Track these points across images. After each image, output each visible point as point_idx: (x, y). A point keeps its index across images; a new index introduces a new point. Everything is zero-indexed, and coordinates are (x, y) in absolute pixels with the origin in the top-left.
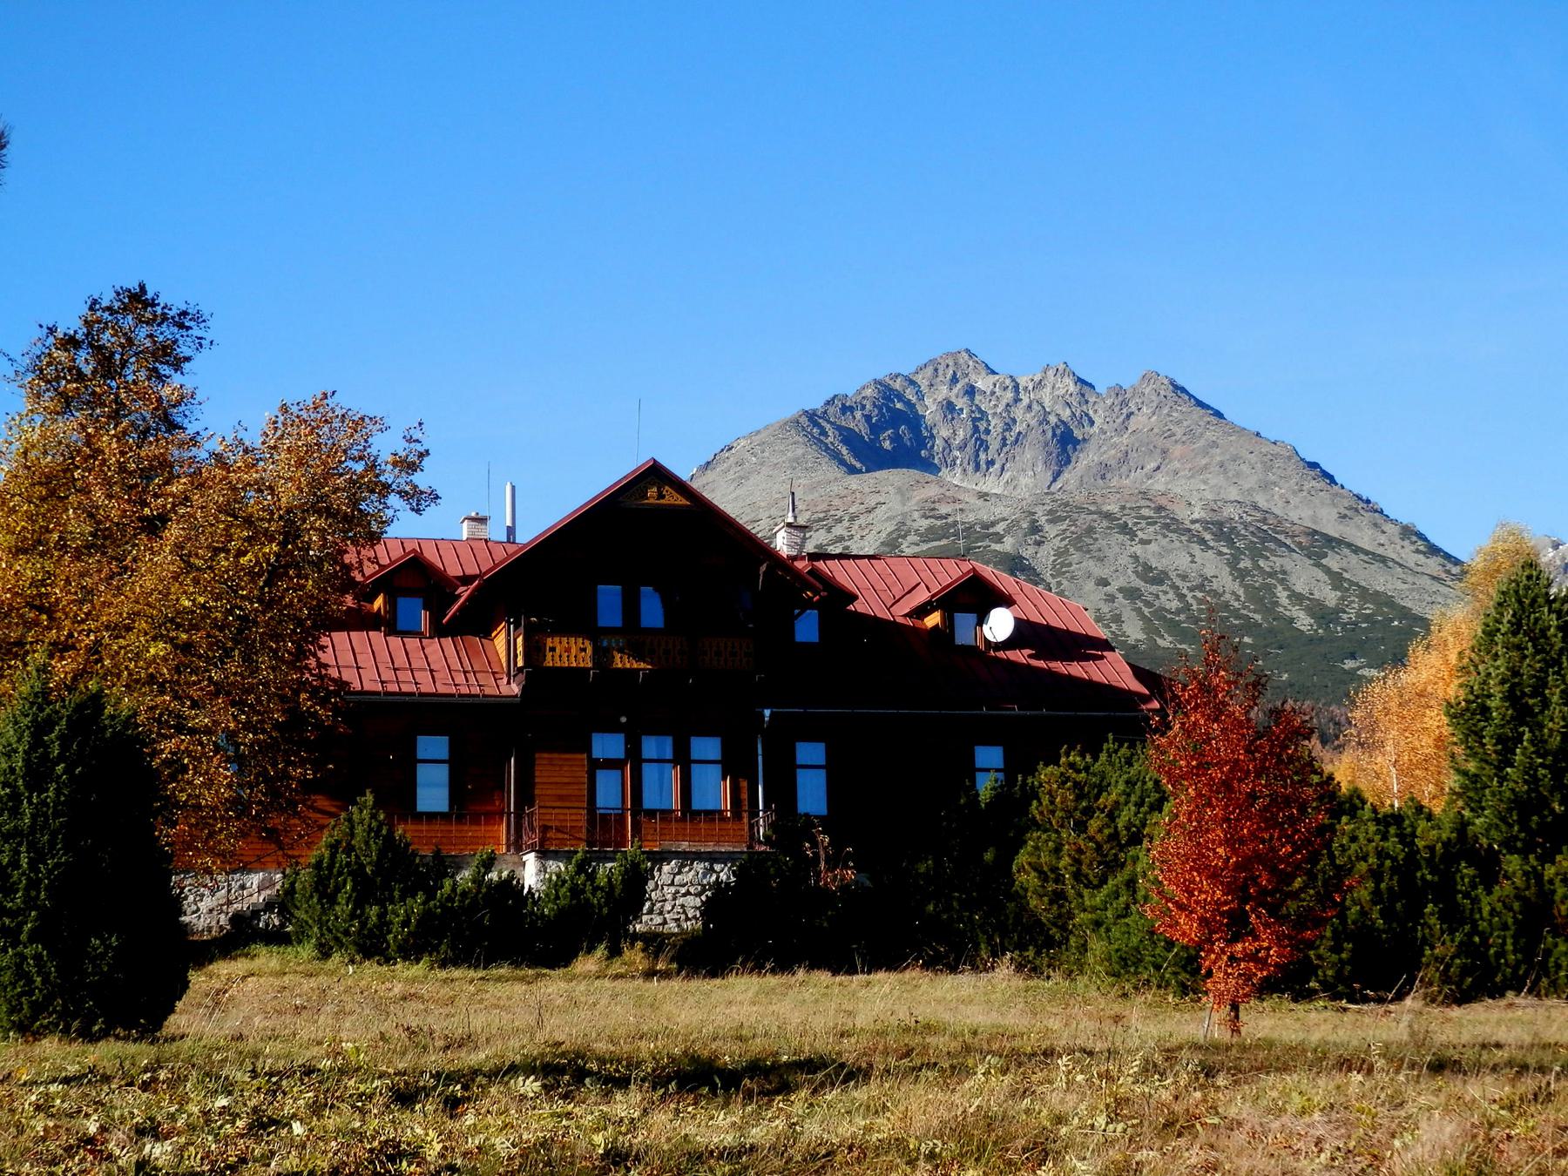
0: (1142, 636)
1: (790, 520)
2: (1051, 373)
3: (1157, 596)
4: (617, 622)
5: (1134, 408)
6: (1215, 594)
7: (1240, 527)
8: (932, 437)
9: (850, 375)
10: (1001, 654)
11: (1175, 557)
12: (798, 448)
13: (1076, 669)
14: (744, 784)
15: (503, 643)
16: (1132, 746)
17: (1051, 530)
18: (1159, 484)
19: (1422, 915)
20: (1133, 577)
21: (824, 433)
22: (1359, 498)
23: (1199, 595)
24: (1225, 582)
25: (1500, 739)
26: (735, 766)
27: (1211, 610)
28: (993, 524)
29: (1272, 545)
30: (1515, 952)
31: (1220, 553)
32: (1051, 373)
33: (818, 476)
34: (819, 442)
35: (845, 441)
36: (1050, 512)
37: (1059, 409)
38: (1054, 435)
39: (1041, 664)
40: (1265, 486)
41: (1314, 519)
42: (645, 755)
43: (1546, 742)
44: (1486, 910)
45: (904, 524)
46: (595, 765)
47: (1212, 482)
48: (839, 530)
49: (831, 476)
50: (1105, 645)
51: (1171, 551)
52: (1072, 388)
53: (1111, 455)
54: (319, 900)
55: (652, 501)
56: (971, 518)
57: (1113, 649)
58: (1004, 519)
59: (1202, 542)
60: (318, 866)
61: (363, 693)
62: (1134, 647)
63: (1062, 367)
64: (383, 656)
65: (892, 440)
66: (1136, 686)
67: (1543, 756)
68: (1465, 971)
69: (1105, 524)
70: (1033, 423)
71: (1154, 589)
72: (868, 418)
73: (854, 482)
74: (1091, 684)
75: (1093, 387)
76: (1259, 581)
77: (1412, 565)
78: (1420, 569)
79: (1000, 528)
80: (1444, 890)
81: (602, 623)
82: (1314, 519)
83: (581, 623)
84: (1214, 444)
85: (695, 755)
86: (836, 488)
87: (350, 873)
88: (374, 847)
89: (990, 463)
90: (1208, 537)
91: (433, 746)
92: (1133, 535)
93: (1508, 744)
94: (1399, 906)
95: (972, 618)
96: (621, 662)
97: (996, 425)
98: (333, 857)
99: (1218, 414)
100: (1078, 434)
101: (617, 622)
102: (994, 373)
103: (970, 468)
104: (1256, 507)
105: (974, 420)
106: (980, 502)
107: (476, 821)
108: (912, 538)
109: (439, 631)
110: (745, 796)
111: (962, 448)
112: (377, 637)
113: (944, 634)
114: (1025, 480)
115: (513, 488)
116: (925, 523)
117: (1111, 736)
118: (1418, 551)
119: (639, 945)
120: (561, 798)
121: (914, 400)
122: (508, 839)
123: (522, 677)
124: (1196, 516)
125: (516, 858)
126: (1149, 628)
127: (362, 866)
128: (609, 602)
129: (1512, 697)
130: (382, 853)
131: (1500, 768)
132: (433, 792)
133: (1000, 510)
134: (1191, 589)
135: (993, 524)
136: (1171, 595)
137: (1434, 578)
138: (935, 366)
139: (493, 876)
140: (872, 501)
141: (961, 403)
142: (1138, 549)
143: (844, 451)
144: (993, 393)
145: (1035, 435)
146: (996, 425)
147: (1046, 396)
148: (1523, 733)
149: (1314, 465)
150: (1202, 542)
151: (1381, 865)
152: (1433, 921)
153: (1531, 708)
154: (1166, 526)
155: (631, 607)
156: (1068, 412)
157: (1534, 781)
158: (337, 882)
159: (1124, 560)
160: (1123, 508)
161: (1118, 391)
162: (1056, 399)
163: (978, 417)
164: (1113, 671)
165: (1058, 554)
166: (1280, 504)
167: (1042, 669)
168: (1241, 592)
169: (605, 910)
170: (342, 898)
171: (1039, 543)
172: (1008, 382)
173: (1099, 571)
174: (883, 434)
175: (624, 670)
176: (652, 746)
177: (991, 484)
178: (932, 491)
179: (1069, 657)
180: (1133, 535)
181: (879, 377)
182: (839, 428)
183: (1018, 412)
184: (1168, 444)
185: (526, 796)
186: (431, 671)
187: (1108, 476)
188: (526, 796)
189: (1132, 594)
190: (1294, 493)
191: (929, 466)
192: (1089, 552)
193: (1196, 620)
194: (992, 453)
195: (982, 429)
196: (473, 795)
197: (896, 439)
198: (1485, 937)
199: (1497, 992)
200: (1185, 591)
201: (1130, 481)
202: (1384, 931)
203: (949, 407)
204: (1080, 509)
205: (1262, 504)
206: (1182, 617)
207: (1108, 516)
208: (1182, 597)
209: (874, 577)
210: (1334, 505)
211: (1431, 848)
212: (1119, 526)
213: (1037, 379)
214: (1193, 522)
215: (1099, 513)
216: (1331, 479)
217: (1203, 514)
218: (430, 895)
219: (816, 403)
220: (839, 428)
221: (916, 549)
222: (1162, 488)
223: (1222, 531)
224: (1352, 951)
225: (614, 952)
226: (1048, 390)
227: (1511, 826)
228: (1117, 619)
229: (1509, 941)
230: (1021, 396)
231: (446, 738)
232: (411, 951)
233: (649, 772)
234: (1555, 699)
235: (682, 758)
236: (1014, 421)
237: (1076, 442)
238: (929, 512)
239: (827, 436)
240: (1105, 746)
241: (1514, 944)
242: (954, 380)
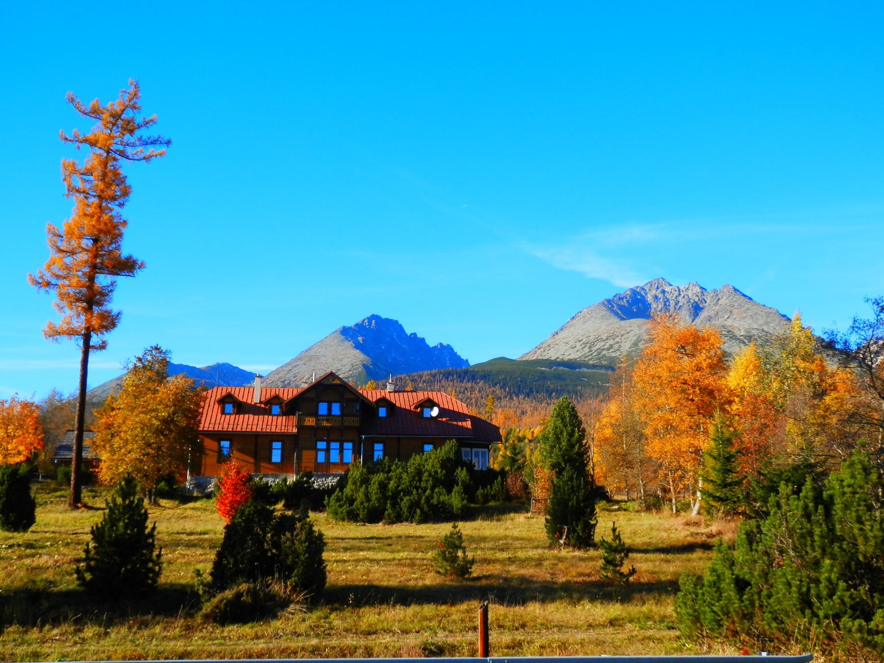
4: (325, 413)
12: (604, 312)
18: (729, 323)
21: (613, 306)
26: (356, 452)
35: (620, 309)
40: (767, 323)
48: (617, 340)
53: (712, 313)
59: (744, 343)
72: (628, 301)
73: (623, 323)
81: (320, 413)
83: (315, 414)
84: (748, 309)
86: (616, 325)
91: (277, 445)
96: (325, 424)
97: (672, 303)
99: (750, 299)
100: (701, 306)
104: (763, 330)
108: (642, 342)
111: (660, 311)
128: (323, 408)
129: (555, 434)
132: (276, 457)
138: (651, 283)
140: (629, 329)
141: (660, 296)
145: (686, 307)
146: (672, 303)
147: (690, 293)
149: (784, 316)
150: (744, 343)
155: (330, 409)
161: (715, 291)
163: (666, 301)
174: (633, 306)
179: (461, 421)
182: (618, 305)
183: (680, 299)
197: (638, 308)
199: (401, 522)
201: (719, 322)
203: (656, 297)
205: (766, 329)
220: (618, 305)
235: (341, 450)
242: (658, 288)
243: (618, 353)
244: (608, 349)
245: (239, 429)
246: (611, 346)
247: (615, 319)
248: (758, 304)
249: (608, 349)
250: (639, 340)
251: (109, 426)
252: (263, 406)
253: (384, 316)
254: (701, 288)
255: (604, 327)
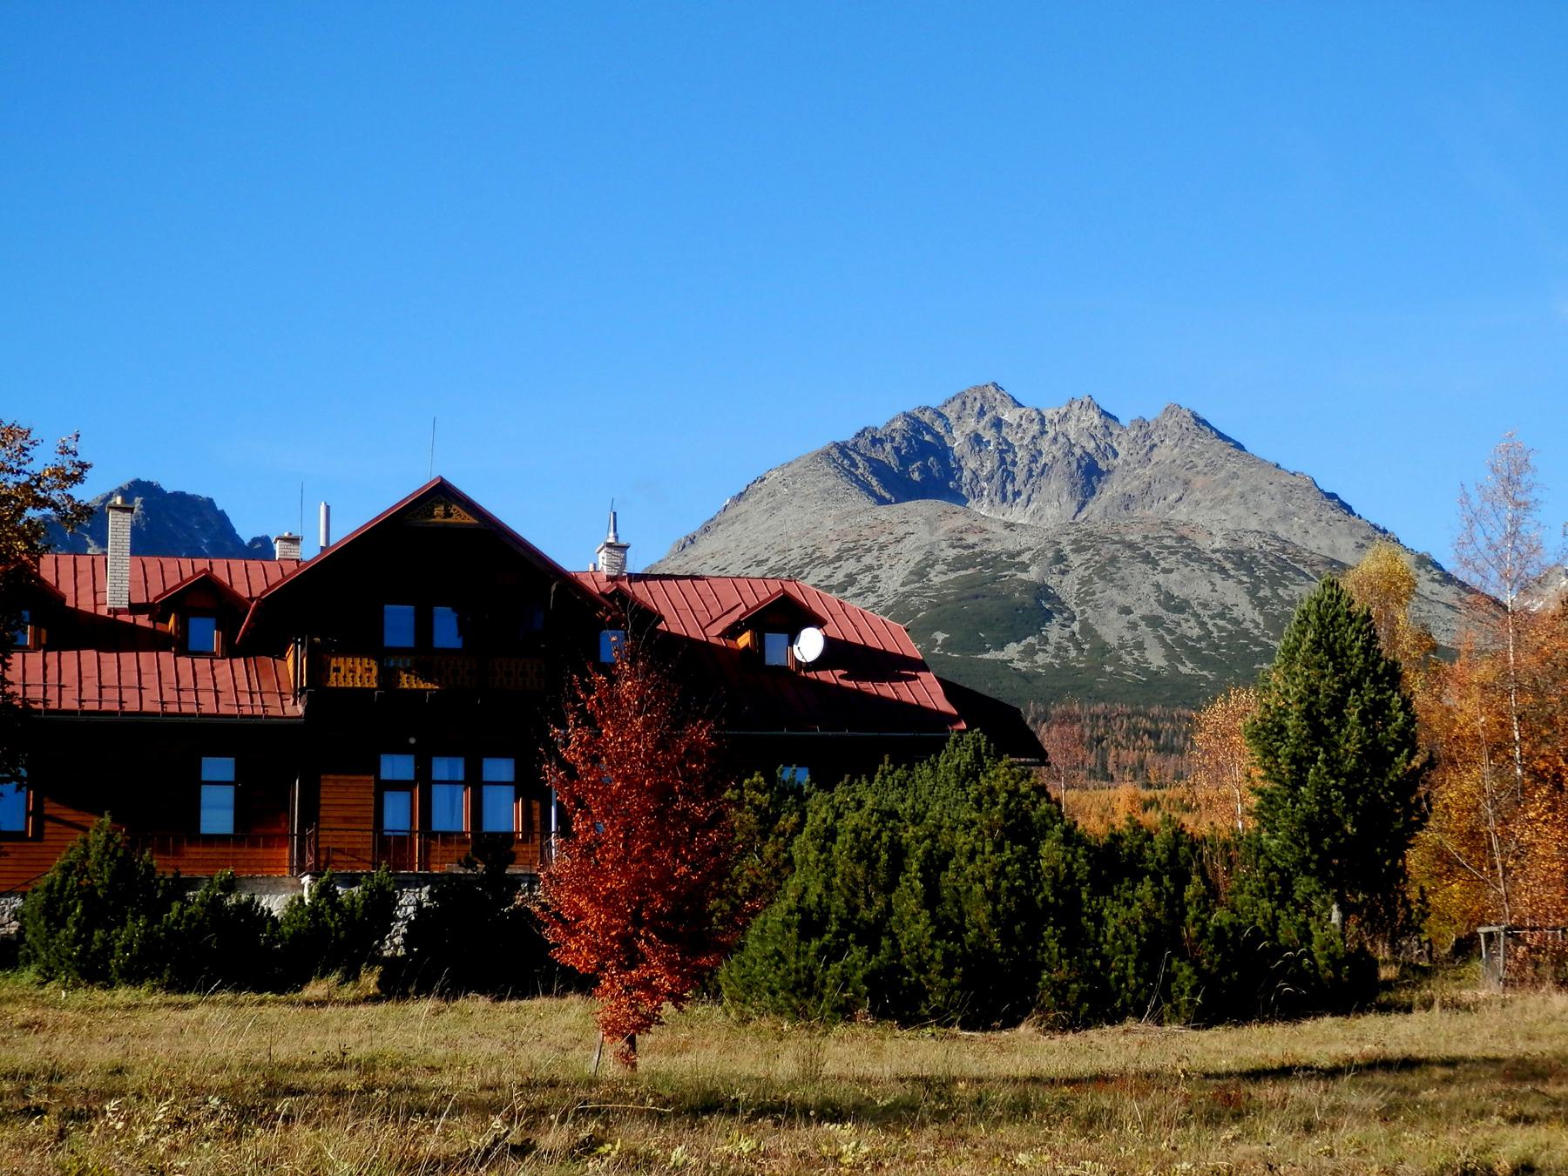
0: (1164, 663)
1: (611, 540)
2: (1076, 406)
3: (1179, 624)
4: (408, 641)
5: (1156, 440)
6: (1236, 622)
7: (1260, 556)
8: (960, 468)
9: (883, 410)
10: (812, 675)
11: (1196, 586)
12: (830, 479)
13: (886, 690)
14: (536, 805)
15: (292, 665)
16: (910, 768)
17: (1075, 560)
18: (1181, 513)
19: (1042, 938)
20: (1155, 605)
21: (854, 464)
22: (1376, 527)
23: (1221, 623)
24: (1245, 610)
25: (1294, 759)
27: (1230, 636)
28: (1019, 553)
29: (1291, 574)
30: (1135, 976)
31: (1240, 582)
32: (1076, 406)
33: (847, 506)
34: (850, 475)
35: (874, 473)
36: (1075, 542)
37: (1084, 441)
38: (1079, 467)
39: (852, 684)
40: (1284, 516)
41: (1333, 549)
42: (436, 776)
43: (1341, 763)
44: (1111, 932)
45: (931, 553)
46: (384, 786)
47: (1234, 512)
48: (868, 560)
49: (860, 507)
50: (921, 666)
51: (1191, 580)
52: (1097, 421)
53: (1134, 486)
54: (47, 925)
55: (438, 519)
56: (998, 548)
57: (926, 669)
58: (1030, 549)
59: (1223, 570)
60: (49, 889)
61: (141, 713)
62: (1157, 673)
63: (1086, 400)
64: (169, 677)
65: (921, 472)
66: (945, 706)
67: (1336, 777)
68: (1083, 996)
69: (1128, 553)
70: (1059, 454)
71: (1175, 617)
72: (897, 450)
73: (883, 512)
74: (900, 705)
75: (1116, 419)
76: (1277, 609)
77: (1427, 594)
78: (1435, 598)
79: (1025, 557)
80: (1068, 910)
82: (1333, 549)
83: (367, 642)
84: (1235, 476)
85: (487, 777)
86: (866, 519)
87: (80, 897)
88: (106, 870)
89: (1017, 494)
90: (1228, 566)
92: (1155, 564)
93: (1300, 763)
94: (1017, 928)
95: (784, 637)
96: (407, 682)
97: (1022, 456)
98: (65, 879)
100: (1102, 465)
101: (408, 641)
102: (1020, 405)
103: (997, 500)
104: (1275, 537)
105: (1001, 452)
106: (1006, 532)
107: (254, 844)
108: (940, 567)
109: (230, 651)
110: (537, 818)
111: (989, 479)
112: (167, 658)
113: (755, 653)
114: (1051, 511)
115: (328, 508)
116: (952, 553)
117: (887, 758)
118: (1433, 580)
119: (378, 969)
120: (346, 820)
121: (942, 432)
122: (291, 860)
123: (304, 697)
124: (1217, 546)
125: (294, 881)
126: (1171, 656)
127: (92, 888)
128: (398, 623)
129: (1309, 715)
130: (114, 876)
131: (1294, 787)
132: (217, 813)
133: (1025, 540)
134: (1212, 617)
135: (1019, 553)
136: (1192, 623)
137: (1448, 606)
138: (963, 399)
139: (231, 901)
140: (900, 531)
141: (989, 435)
142: (1161, 578)
143: (874, 482)
144: (1020, 426)
145: (1060, 467)
146: (1022, 456)
147: (1071, 428)
148: (1317, 754)
149: (1332, 496)
150: (1223, 570)
151: (997, 886)
152: (1052, 944)
153: (1327, 728)
154: (1188, 556)
155: (424, 627)
156: (1093, 444)
157: (1325, 800)
158: (66, 907)
159: (1147, 588)
160: (1146, 537)
161: (1142, 423)
162: (1080, 432)
163: (1005, 449)
164: (926, 692)
165: (1083, 582)
166: (1299, 533)
167: (851, 689)
168: (1260, 619)
169: (342, 934)
170: (70, 920)
171: (1063, 573)
172: (1034, 414)
173: (1121, 599)
174: (913, 466)
175: (411, 691)
176: (443, 768)
177: (1017, 515)
178: (960, 521)
180: (1155, 564)
181: (909, 409)
182: (869, 460)
183: (1044, 444)
184: (1189, 475)
185: (310, 814)
186: (217, 692)
187: (1132, 506)
188: (310, 814)
189: (1154, 622)
190: (1313, 522)
191: (957, 497)
192: (1112, 581)
193: (1217, 647)
194: (1018, 484)
195: (1009, 460)
196: (258, 819)
197: (925, 470)
198: (1106, 961)
199: (1115, 1018)
200: (1206, 619)
201: (1152, 512)
202: (1001, 955)
203: (977, 439)
204: (1104, 539)
205: (1282, 533)
206: (1203, 644)
207: (1131, 546)
208: (1203, 625)
209: (693, 597)
210: (1352, 535)
211: (1054, 869)
212: (1142, 556)
213: (1062, 411)
214: (1214, 551)
215: (1122, 542)
216: (1349, 510)
217: (1224, 544)
218: (154, 918)
219: (847, 436)
220: (869, 460)
221: (944, 578)
222: (1184, 518)
223: (1242, 559)
224: (962, 975)
225: (351, 975)
226: (1073, 422)
227: (1303, 847)
228: (1140, 646)
229: (1131, 965)
230: (1047, 428)
231: (231, 760)
232: (133, 976)
233: (439, 793)
234: (1354, 718)
235: (474, 780)
236: (1040, 453)
237: (1100, 473)
238: (957, 542)
239: (857, 467)
240: (880, 767)
241: (1136, 968)
242: (982, 413)
243: (872, 599)
244: (842, 588)
245: (70, 703)
246: (851, 579)
247: (865, 502)
248: (1262, 462)
249: (842, 588)
250: (929, 561)
251: (23, 449)
252: (143, 620)
253: (169, 488)
254: (1104, 413)
255: (829, 523)
